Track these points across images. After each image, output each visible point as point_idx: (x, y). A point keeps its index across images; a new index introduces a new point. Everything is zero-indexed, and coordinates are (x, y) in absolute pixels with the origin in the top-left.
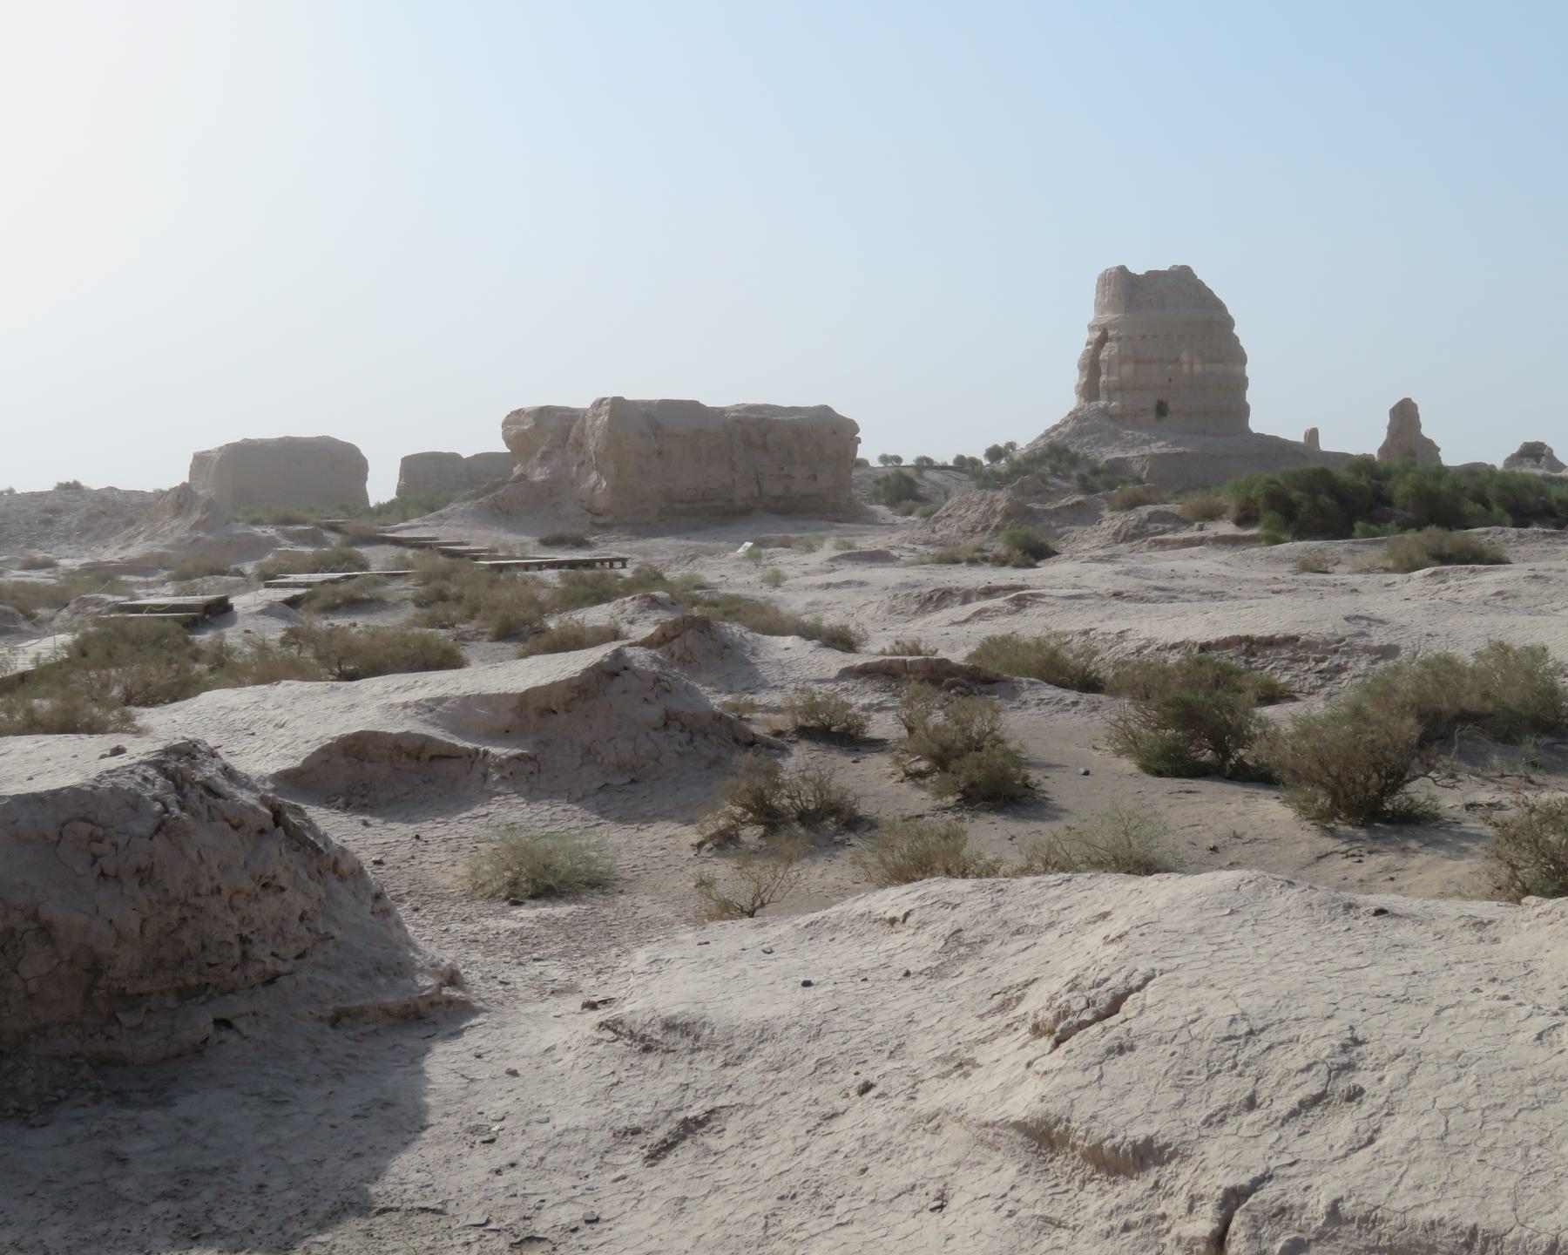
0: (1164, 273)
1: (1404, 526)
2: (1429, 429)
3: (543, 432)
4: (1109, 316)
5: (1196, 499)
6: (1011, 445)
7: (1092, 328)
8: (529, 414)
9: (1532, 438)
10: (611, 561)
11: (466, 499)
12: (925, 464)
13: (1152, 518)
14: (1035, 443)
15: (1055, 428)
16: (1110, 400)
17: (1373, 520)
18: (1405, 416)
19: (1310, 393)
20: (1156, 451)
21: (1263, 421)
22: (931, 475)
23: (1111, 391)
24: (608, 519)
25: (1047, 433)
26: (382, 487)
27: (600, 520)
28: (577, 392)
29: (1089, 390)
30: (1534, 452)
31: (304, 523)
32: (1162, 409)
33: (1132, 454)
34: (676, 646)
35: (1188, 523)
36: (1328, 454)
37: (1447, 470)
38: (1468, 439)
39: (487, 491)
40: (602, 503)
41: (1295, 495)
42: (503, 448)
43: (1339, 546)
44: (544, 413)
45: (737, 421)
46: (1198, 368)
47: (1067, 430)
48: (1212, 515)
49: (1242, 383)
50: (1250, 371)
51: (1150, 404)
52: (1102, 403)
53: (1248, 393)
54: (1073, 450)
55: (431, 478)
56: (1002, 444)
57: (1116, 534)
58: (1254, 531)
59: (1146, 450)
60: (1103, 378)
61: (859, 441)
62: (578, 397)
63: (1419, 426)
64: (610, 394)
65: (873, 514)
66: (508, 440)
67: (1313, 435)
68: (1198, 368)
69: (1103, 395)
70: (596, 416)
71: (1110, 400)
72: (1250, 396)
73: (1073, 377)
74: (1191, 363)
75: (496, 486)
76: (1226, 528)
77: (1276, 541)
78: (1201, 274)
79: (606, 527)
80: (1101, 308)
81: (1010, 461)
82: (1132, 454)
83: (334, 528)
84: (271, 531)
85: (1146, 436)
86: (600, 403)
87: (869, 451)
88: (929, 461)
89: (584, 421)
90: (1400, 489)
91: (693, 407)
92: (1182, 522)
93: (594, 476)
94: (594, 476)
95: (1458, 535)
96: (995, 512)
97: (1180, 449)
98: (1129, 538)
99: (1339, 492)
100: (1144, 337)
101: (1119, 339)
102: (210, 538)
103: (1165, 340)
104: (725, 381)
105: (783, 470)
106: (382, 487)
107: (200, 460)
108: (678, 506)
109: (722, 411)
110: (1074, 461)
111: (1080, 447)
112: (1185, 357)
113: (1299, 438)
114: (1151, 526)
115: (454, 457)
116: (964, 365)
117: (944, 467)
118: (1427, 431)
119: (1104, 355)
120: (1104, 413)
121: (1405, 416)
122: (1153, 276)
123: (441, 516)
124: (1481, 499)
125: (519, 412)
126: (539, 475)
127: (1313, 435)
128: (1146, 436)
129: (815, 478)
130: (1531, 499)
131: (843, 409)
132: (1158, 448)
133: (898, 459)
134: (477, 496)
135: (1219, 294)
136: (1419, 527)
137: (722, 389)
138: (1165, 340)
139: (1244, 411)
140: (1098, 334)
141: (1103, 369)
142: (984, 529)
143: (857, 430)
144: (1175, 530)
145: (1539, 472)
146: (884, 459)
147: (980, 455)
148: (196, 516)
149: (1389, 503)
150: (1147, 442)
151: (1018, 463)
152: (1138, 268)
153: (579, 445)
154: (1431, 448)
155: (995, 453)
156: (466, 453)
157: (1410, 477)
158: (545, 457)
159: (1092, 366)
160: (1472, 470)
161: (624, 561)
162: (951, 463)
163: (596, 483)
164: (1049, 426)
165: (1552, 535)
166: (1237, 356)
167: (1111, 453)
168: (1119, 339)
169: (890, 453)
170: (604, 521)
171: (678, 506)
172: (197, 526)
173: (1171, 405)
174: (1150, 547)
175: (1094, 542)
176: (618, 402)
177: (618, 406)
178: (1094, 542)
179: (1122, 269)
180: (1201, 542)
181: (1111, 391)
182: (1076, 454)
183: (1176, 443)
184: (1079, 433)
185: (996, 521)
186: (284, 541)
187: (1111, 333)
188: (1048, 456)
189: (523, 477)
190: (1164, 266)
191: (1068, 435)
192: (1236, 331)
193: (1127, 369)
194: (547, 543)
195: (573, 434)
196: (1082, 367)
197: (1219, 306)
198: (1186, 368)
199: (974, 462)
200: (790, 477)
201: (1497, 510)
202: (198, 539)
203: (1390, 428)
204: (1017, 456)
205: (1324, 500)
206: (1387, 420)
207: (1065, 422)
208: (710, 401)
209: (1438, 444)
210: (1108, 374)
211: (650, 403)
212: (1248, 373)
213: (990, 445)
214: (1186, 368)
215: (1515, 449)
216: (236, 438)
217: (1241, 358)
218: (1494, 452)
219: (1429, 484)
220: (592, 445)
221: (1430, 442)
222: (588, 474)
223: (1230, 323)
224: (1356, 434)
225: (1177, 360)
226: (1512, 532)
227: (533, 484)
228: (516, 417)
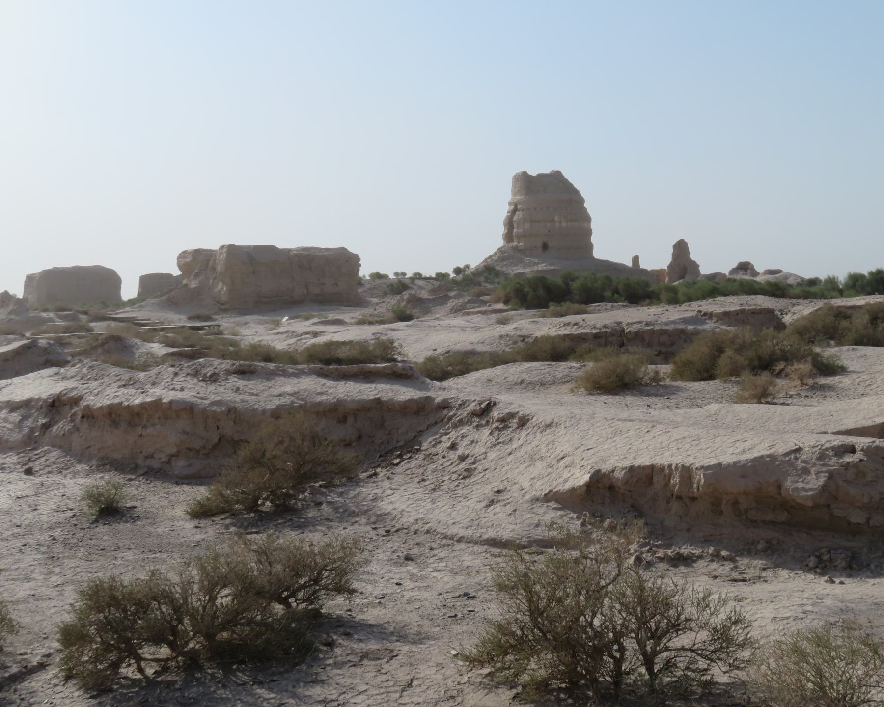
0: (546, 175)
3: (197, 262)
4: (518, 198)
6: (467, 266)
7: (510, 204)
8: (190, 253)
9: (743, 260)
11: (155, 297)
12: (418, 276)
14: (479, 265)
15: (490, 257)
16: (519, 242)
18: (681, 248)
19: (617, 240)
20: (540, 268)
21: (598, 253)
22: (420, 283)
23: (519, 237)
24: (227, 306)
25: (486, 260)
26: (129, 290)
27: (223, 307)
28: (212, 240)
29: (509, 237)
30: (744, 267)
31: (70, 310)
32: (545, 247)
34: (106, 347)
39: (166, 293)
40: (224, 298)
41: (527, 289)
42: (176, 272)
44: (197, 253)
45: (296, 255)
47: (495, 258)
49: (589, 232)
50: (593, 226)
52: (515, 244)
54: (497, 268)
55: (152, 285)
56: (462, 266)
57: (451, 310)
59: (535, 268)
60: (515, 230)
61: (360, 265)
62: (214, 245)
63: (689, 253)
64: (228, 243)
66: (180, 267)
67: (636, 259)
68: (564, 225)
70: (221, 254)
71: (519, 242)
72: (594, 239)
73: (501, 230)
74: (560, 222)
75: (171, 290)
78: (566, 175)
79: (225, 311)
80: (514, 194)
81: (464, 276)
83: (85, 313)
84: (51, 315)
85: (536, 260)
86: (223, 247)
87: (365, 272)
88: (420, 275)
91: (272, 249)
93: (220, 285)
94: (220, 285)
97: (553, 267)
100: (536, 208)
101: (523, 210)
102: (17, 318)
103: (548, 207)
104: (290, 235)
106: (129, 290)
109: (289, 251)
110: (497, 274)
111: (502, 267)
112: (557, 218)
114: (468, 306)
118: (693, 256)
119: (515, 218)
120: (516, 249)
121: (681, 248)
122: (541, 176)
123: (141, 306)
125: (185, 252)
126: (194, 284)
128: (536, 260)
129: (336, 284)
131: (352, 249)
133: (404, 274)
134: (161, 296)
137: (289, 239)
138: (548, 207)
139: (590, 247)
141: (515, 226)
143: (359, 260)
146: (396, 274)
148: (11, 307)
150: (537, 264)
151: (467, 276)
152: (533, 173)
154: (695, 266)
155: (458, 271)
159: (510, 224)
162: (434, 276)
163: (221, 288)
164: (487, 256)
165: (626, 306)
168: (523, 210)
169: (399, 271)
170: (225, 308)
172: (10, 313)
173: (550, 245)
174: (463, 315)
177: (232, 250)
179: (525, 173)
181: (519, 237)
182: (498, 271)
183: (552, 264)
186: (57, 320)
187: (519, 207)
189: (186, 285)
190: (547, 171)
191: (496, 261)
192: (586, 205)
193: (527, 226)
194: (190, 318)
195: (211, 262)
196: (505, 225)
197: (576, 192)
198: (557, 225)
200: (324, 284)
202: (11, 319)
203: (673, 255)
204: (468, 272)
206: (671, 251)
207: (496, 254)
208: (281, 246)
209: (698, 263)
210: (518, 228)
211: (249, 247)
213: (455, 266)
214: (557, 225)
215: (735, 265)
216: (49, 266)
217: (588, 219)
218: (725, 266)
220: (219, 268)
221: (694, 262)
222: (217, 284)
223: (582, 201)
224: (657, 259)
228: (183, 255)
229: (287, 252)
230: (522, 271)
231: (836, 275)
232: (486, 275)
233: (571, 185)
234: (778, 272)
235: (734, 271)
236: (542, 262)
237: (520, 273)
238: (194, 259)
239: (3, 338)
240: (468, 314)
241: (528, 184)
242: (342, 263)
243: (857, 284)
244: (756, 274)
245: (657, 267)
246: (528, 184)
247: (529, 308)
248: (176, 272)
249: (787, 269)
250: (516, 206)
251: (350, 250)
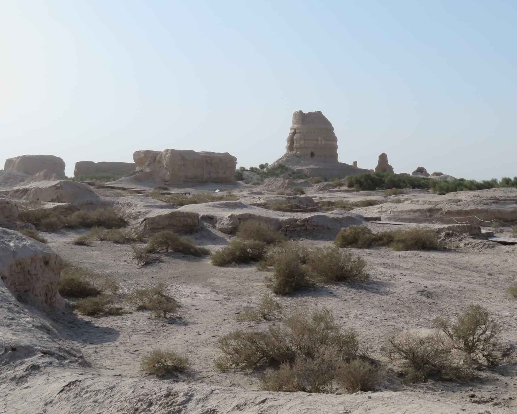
1: (387, 188)
2: (390, 162)
4: (297, 126)
5: (336, 181)
6: (267, 164)
7: (291, 129)
9: (420, 167)
10: (185, 194)
11: (126, 176)
13: (327, 185)
15: (280, 159)
16: (297, 151)
17: (380, 187)
18: (383, 158)
19: (356, 151)
20: (311, 167)
22: (245, 172)
23: (297, 149)
25: (278, 161)
29: (291, 148)
30: (421, 170)
32: (312, 155)
33: (304, 168)
35: (335, 187)
36: (341, 164)
37: (396, 175)
38: (402, 166)
40: (167, 178)
41: (363, 180)
43: (374, 192)
45: (204, 156)
46: (323, 142)
47: (284, 160)
48: (340, 185)
49: (336, 147)
50: (338, 143)
51: (309, 153)
52: (294, 152)
53: (338, 150)
54: (286, 166)
56: (264, 164)
57: (318, 189)
58: (353, 189)
60: (295, 144)
63: (387, 161)
64: (170, 148)
65: (239, 183)
67: (355, 163)
68: (323, 142)
69: (294, 149)
70: (166, 154)
71: (297, 151)
72: (338, 151)
73: (285, 144)
74: (321, 141)
76: (346, 188)
77: (358, 191)
78: (324, 114)
80: (294, 123)
81: (268, 169)
82: (304, 168)
88: (244, 168)
89: (161, 155)
90: (386, 180)
91: (192, 152)
92: (335, 187)
95: (400, 190)
96: (285, 183)
97: (318, 167)
98: (322, 190)
99: (373, 180)
100: (307, 132)
101: (300, 133)
105: (214, 171)
107: (9, 162)
108: (188, 180)
110: (287, 169)
112: (319, 139)
113: (351, 163)
115: (92, 163)
116: (258, 142)
117: (247, 170)
118: (390, 163)
119: (295, 137)
120: (295, 155)
121: (383, 158)
122: (310, 114)
123: (120, 181)
124: (404, 182)
126: (148, 170)
127: (355, 163)
129: (225, 173)
130: (416, 183)
131: (232, 154)
132: (311, 166)
134: (130, 175)
135: (329, 120)
136: (391, 188)
137: (200, 147)
139: (336, 156)
140: (293, 131)
141: (295, 142)
142: (283, 187)
143: (236, 160)
144: (333, 188)
145: (421, 176)
147: (258, 167)
149: (384, 183)
150: (308, 165)
152: (306, 112)
153: (159, 162)
154: (391, 169)
155: (262, 167)
156: (96, 162)
157: (389, 177)
158: (149, 165)
159: (291, 141)
160: (403, 175)
161: (189, 194)
164: (278, 158)
166: (335, 139)
167: (297, 168)
168: (300, 133)
171: (188, 180)
173: (315, 153)
174: (328, 192)
175: (313, 191)
176: (173, 150)
177: (173, 152)
178: (313, 191)
179: (301, 112)
180: (340, 191)
183: (316, 165)
184: (287, 161)
185: (286, 185)
187: (297, 131)
188: (279, 168)
190: (313, 111)
192: (334, 131)
196: (288, 141)
197: (329, 124)
198: (320, 142)
199: (256, 169)
200: (218, 172)
201: (408, 185)
204: (269, 168)
205: (369, 181)
206: (378, 159)
208: (197, 151)
210: (296, 143)
211: (181, 151)
212: (338, 144)
214: (320, 142)
215: (415, 169)
217: (335, 139)
219: (393, 178)
220: (165, 162)
221: (390, 166)
223: (332, 129)
224: (369, 164)
225: (317, 140)
226: (411, 190)
227: (146, 172)
229: (198, 154)
230: (301, 168)
231: (494, 178)
232: (280, 169)
233: (327, 119)
234: (440, 174)
235: (415, 173)
236: (311, 164)
237: (300, 169)
238: (145, 156)
239: (516, 198)
240: (331, 191)
241: (302, 118)
242: (228, 161)
243: (507, 182)
244: (428, 175)
245: (368, 168)
246: (302, 118)
247: (364, 189)
248: (238, 167)
249: (445, 173)
250: (295, 130)
251: (231, 154)
